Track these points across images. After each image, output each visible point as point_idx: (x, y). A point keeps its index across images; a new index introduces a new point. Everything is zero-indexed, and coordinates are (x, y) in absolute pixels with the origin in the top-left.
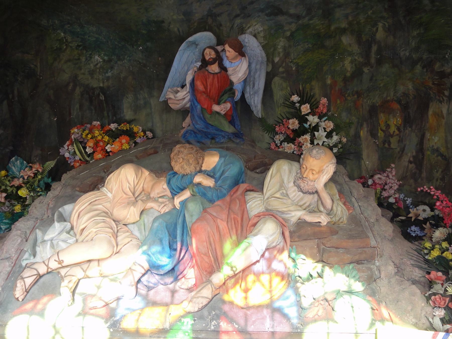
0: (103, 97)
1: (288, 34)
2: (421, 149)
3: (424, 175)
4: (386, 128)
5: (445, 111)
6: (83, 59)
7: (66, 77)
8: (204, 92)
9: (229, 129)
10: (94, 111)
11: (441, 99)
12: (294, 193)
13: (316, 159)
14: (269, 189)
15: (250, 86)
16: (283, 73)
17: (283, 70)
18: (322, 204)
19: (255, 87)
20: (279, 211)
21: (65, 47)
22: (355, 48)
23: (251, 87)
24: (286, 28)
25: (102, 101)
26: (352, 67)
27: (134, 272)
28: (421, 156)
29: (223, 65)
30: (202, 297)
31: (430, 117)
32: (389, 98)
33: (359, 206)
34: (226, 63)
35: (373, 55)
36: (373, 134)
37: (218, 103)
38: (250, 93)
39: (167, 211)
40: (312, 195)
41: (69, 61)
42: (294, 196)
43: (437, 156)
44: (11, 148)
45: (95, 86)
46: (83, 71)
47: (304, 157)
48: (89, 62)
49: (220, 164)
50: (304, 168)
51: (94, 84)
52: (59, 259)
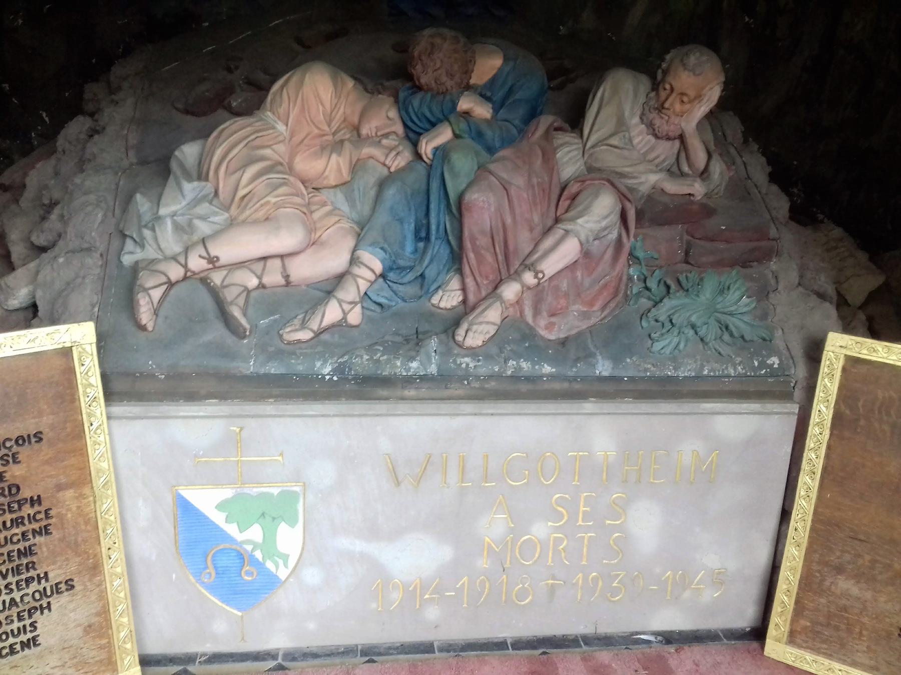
12: (641, 138)
13: (694, 74)
18: (688, 158)
20: (617, 173)
30: (488, 323)
33: (745, 164)
39: (403, 164)
40: (671, 142)
42: (639, 143)
50: (665, 89)
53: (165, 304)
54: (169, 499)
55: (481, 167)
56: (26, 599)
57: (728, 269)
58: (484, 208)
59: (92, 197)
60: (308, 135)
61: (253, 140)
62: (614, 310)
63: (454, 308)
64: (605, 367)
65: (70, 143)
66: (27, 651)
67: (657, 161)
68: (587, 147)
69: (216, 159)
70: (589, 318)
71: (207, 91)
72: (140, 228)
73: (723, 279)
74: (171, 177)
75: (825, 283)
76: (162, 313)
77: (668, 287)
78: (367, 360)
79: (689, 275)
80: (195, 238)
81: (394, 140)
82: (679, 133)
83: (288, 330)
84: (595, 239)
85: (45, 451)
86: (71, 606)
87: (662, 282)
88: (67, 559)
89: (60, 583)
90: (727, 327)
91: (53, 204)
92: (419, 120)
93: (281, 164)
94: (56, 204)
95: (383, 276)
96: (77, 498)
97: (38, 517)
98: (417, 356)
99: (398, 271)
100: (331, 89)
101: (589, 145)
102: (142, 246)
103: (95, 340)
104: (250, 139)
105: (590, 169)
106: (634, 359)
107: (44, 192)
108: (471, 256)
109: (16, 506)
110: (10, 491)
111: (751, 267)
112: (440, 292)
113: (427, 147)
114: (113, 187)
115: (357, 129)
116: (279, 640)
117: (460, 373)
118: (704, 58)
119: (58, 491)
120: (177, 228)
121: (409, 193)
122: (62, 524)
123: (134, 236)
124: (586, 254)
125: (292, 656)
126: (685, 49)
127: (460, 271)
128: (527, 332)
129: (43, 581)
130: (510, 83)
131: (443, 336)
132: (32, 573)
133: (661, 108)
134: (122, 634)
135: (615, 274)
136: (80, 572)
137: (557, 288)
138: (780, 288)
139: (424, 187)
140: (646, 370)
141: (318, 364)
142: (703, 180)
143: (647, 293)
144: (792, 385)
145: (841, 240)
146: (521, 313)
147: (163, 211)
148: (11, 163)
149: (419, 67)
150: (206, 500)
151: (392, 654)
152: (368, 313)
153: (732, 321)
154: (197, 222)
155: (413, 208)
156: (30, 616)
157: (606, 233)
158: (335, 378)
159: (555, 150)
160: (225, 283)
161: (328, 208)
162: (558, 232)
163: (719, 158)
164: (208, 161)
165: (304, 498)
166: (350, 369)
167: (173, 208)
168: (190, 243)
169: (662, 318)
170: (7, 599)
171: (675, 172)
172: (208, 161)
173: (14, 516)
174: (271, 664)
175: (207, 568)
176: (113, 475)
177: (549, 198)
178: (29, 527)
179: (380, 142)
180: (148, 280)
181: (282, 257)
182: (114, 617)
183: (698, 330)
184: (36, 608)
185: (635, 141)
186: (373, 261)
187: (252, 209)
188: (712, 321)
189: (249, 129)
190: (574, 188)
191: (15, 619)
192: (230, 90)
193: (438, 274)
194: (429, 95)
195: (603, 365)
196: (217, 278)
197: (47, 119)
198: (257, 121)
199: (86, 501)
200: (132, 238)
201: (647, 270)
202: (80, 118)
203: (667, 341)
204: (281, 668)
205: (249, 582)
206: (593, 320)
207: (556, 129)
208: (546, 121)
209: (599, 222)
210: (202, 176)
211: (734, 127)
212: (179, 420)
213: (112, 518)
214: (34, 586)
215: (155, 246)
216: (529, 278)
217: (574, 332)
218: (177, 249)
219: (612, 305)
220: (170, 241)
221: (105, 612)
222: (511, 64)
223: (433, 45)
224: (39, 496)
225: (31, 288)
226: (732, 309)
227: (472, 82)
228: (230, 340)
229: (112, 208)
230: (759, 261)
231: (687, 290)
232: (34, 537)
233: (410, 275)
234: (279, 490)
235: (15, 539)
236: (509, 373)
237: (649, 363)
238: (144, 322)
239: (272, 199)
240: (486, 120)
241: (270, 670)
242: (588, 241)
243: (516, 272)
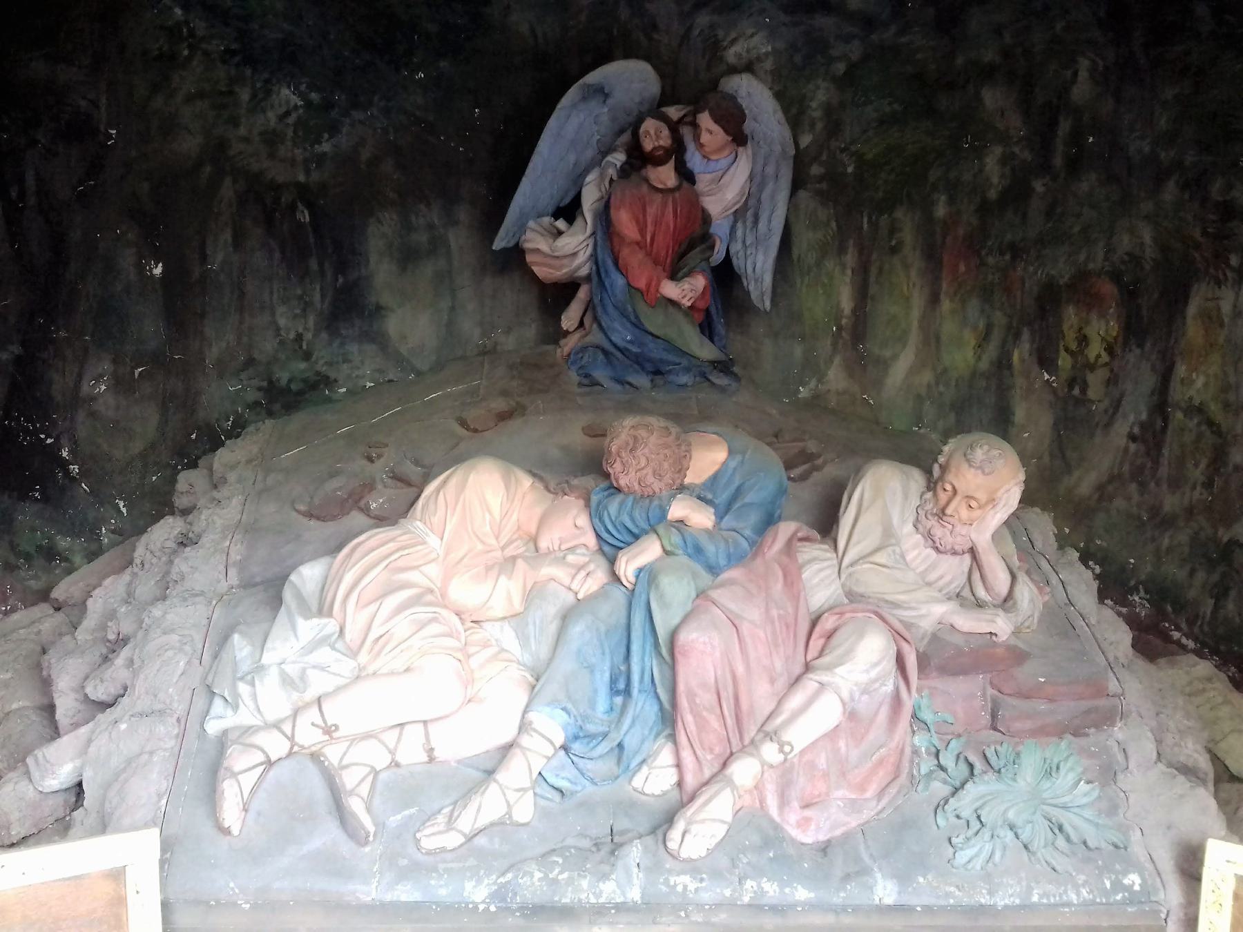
0: (306, 213)
1: (840, 68)
2: (1161, 405)
3: (1164, 471)
4: (1080, 344)
5: (1226, 308)
6: (245, 95)
7: (189, 144)
8: (638, 243)
9: (705, 351)
10: (277, 255)
11: (1221, 277)
13: (983, 472)
14: (854, 538)
15: (744, 222)
16: (821, 179)
17: (822, 170)
19: (760, 225)
21: (186, 52)
22: (1015, 123)
23: (749, 223)
24: (835, 53)
25: (301, 225)
26: (1002, 176)
27: (528, 753)
28: (1159, 423)
29: (684, 163)
31: (1189, 321)
32: (1091, 266)
34: (694, 160)
35: (1060, 147)
36: (1045, 360)
37: (674, 276)
38: (744, 242)
39: (595, 588)
40: (958, 557)
41: (201, 95)
42: (916, 558)
43: (1199, 424)
44: (16, 349)
45: (280, 179)
46: (242, 131)
47: (948, 462)
48: (263, 104)
49: (730, 471)
51: (279, 173)
52: (325, 721)
53: (261, 794)
55: (701, 594)
57: (1055, 739)
58: (705, 652)
59: (174, 638)
62: (894, 798)
63: (665, 793)
64: (887, 892)
67: (941, 583)
68: (844, 564)
70: (860, 811)
71: (340, 489)
72: (236, 679)
73: (1048, 754)
74: (283, 608)
75: (1193, 752)
76: (255, 806)
77: (971, 766)
78: (540, 880)
79: (999, 748)
81: (584, 555)
82: (969, 545)
83: (427, 831)
84: (862, 693)
87: (962, 757)
90: (1061, 828)
91: (122, 641)
92: (618, 531)
93: (431, 591)
95: (565, 748)
98: (611, 873)
99: (585, 741)
100: (502, 491)
101: (846, 561)
102: (235, 708)
105: (852, 596)
106: (930, 877)
107: (110, 624)
108: (689, 718)
111: (1087, 735)
112: (645, 769)
113: (628, 566)
114: (205, 622)
115: (534, 540)
117: (673, 899)
118: (996, 452)
121: (603, 629)
123: (226, 695)
124: (851, 715)
126: (969, 438)
127: (673, 738)
128: (771, 833)
130: (737, 483)
131: (649, 840)
133: (941, 514)
135: (893, 745)
137: (812, 765)
138: (1132, 765)
139: (623, 621)
140: (948, 895)
141: (469, 885)
142: (1006, 611)
143: (943, 775)
144: (1163, 916)
145: (1209, 680)
146: (762, 807)
147: (268, 658)
149: (618, 466)
152: (542, 802)
153: (1066, 818)
155: (607, 651)
157: (877, 685)
159: (800, 568)
160: (344, 762)
161: (490, 652)
162: (810, 684)
163: (1026, 578)
166: (515, 894)
168: (300, 704)
169: (967, 813)
171: (968, 600)
177: (795, 636)
179: (564, 558)
180: (239, 759)
181: (425, 722)
183: (1020, 831)
185: (909, 558)
186: (551, 725)
188: (1038, 817)
190: (828, 623)
192: (369, 486)
193: (643, 742)
194: (631, 498)
195: (885, 888)
196: (333, 754)
197: (124, 510)
198: (405, 534)
201: (941, 739)
202: (169, 520)
203: (975, 850)
206: (866, 815)
207: (801, 540)
208: (786, 529)
209: (867, 671)
210: (324, 610)
211: (1043, 526)
216: (770, 751)
217: (838, 832)
219: (893, 790)
222: (739, 458)
223: (635, 438)
225: (78, 763)
226: (1066, 799)
227: (687, 481)
228: (346, 847)
230: (1097, 726)
231: (999, 772)
233: (604, 744)
236: (746, 899)
237: (951, 885)
240: (707, 531)
242: (852, 699)
243: (752, 742)
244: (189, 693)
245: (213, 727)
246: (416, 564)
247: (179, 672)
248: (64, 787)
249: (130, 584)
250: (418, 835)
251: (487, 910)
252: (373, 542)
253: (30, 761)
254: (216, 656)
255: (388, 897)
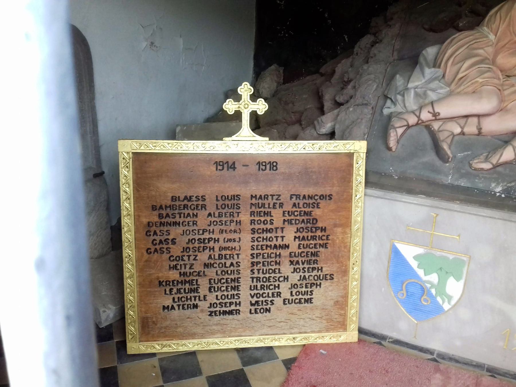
53: (404, 138)
54: (388, 246)
56: (311, 278)
59: (372, 76)
60: (510, 41)
61: (472, 44)
65: (361, 49)
66: (306, 304)
69: (447, 55)
74: (418, 66)
76: (401, 142)
80: (427, 101)
83: (475, 161)
85: (332, 205)
86: (331, 288)
88: (333, 264)
89: (327, 274)
93: (489, 59)
94: (350, 81)
96: (343, 233)
97: (323, 238)
103: (366, 151)
104: (471, 43)
107: (345, 75)
109: (314, 229)
110: (313, 221)
114: (384, 71)
116: (436, 345)
119: (335, 227)
120: (417, 95)
122: (334, 244)
123: (393, 98)
125: (443, 356)
129: (320, 271)
132: (315, 266)
134: (352, 311)
136: (337, 272)
141: (493, 185)
147: (410, 85)
148: (326, 63)
150: (409, 252)
151: (507, 377)
154: (430, 93)
156: (311, 287)
158: (503, 196)
160: (440, 129)
164: (441, 57)
165: (468, 266)
167: (417, 84)
168: (423, 104)
170: (303, 275)
172: (441, 57)
173: (313, 234)
174: (430, 357)
175: (402, 290)
176: (362, 225)
178: (319, 242)
180: (396, 123)
181: (478, 116)
182: (350, 301)
184: (314, 284)
187: (466, 85)
189: (471, 37)
191: (304, 286)
192: (459, 17)
196: (436, 126)
197: (347, 39)
199: (347, 235)
200: (391, 99)
202: (369, 36)
204: (435, 360)
205: (425, 306)
212: (402, 203)
213: (358, 248)
214: (315, 273)
215: (402, 105)
218: (415, 107)
220: (411, 102)
221: (346, 297)
224: (325, 227)
225: (333, 123)
228: (438, 162)
229: (381, 83)
232: (320, 248)
234: (454, 256)
235: (311, 246)
238: (391, 145)
239: (480, 80)
241: (428, 359)
244: (377, 98)
245: (386, 111)
246: (481, 47)
247: (373, 90)
248: (327, 132)
249: (352, 61)
250: (471, 162)
251: (500, 196)
252: (461, 37)
253: (316, 122)
254: (388, 85)
255: (456, 183)
